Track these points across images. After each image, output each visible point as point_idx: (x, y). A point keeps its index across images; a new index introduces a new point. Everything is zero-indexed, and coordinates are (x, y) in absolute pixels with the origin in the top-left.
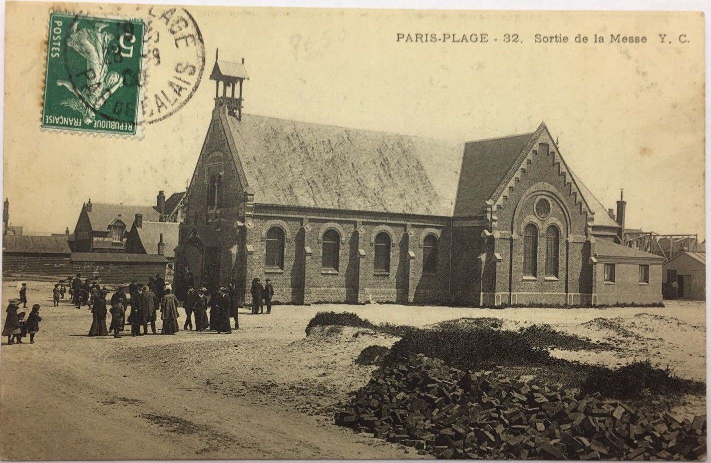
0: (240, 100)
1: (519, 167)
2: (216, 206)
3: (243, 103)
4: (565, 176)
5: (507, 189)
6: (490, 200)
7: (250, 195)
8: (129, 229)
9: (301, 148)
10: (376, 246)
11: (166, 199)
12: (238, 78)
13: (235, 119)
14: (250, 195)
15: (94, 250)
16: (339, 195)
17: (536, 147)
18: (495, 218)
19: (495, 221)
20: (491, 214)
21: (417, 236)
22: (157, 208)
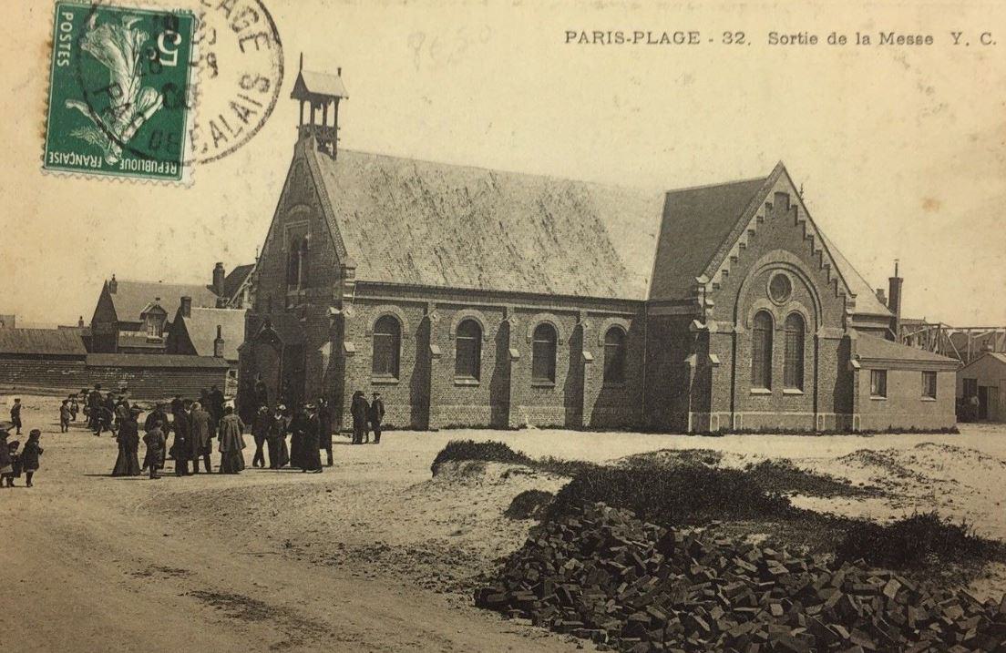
0: (335, 129)
3: (339, 134)
4: (813, 241)
5: (727, 260)
6: (703, 276)
7: (350, 269)
9: (425, 199)
11: (226, 275)
13: (327, 158)
15: (120, 350)
16: (481, 269)
17: (770, 198)
18: (710, 302)
19: (711, 306)
21: (597, 330)
22: (214, 288)
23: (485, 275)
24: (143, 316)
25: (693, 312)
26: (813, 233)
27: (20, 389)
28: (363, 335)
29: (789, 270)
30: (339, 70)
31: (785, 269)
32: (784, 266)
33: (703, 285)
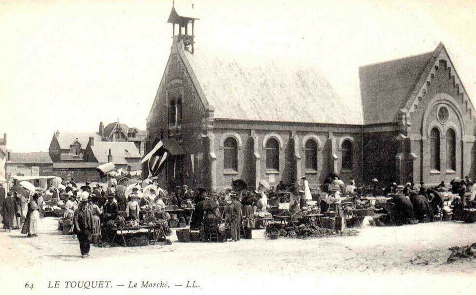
0: (192, 37)
1: (425, 80)
2: (176, 123)
3: (195, 40)
4: (458, 87)
5: (417, 99)
6: (404, 109)
7: (211, 111)
8: (84, 147)
9: (241, 74)
10: (306, 151)
11: (105, 127)
12: (190, 19)
13: (189, 53)
14: (211, 111)
15: (62, 161)
16: (276, 110)
17: (437, 63)
18: (409, 123)
19: (409, 126)
20: (406, 120)
21: (337, 142)
22: (100, 133)
23: (279, 114)
24: (71, 146)
25: (398, 129)
26: (459, 83)
27: (282, 219)
28: (218, 148)
29: (448, 105)
30: (193, 5)
31: (446, 104)
32: (444, 102)
33: (405, 114)
